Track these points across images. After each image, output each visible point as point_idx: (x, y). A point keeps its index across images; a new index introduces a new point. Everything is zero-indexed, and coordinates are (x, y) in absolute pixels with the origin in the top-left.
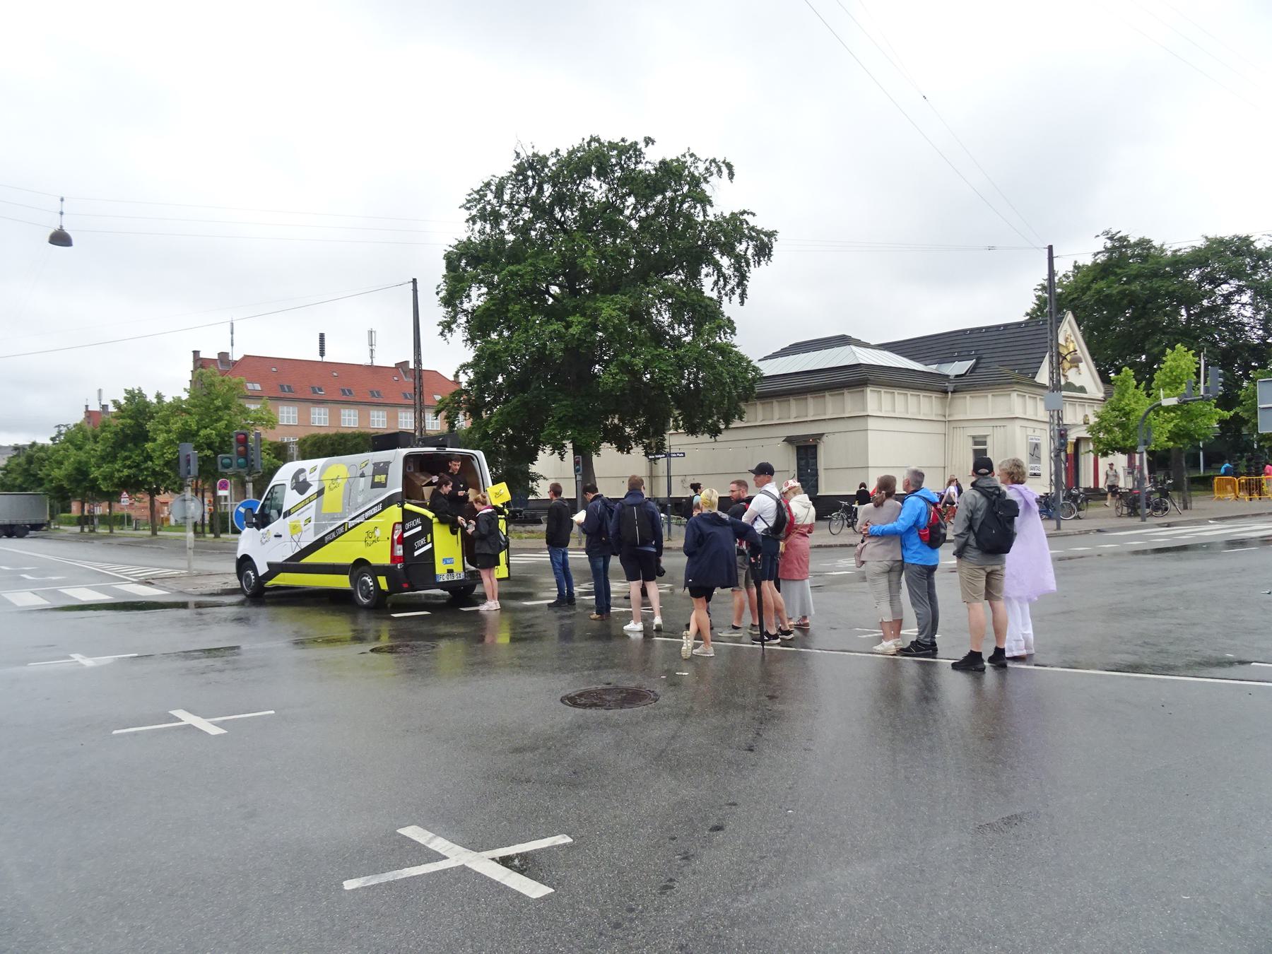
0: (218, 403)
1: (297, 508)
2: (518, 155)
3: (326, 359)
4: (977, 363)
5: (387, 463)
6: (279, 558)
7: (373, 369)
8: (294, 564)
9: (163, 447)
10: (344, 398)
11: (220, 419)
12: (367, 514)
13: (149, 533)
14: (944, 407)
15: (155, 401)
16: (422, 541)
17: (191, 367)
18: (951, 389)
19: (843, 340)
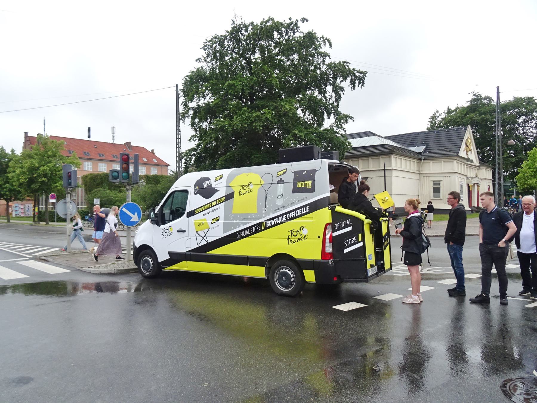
0: (50, 153)
1: (201, 209)
2: (234, 22)
3: (91, 139)
4: (426, 148)
5: (314, 171)
6: (183, 249)
7: (114, 145)
8: (200, 254)
9: (19, 175)
10: (99, 158)
11: (50, 162)
12: (290, 216)
13: (6, 221)
14: (419, 166)
15: (10, 153)
16: (353, 240)
17: (23, 140)
18: (423, 158)
19: (369, 134)
